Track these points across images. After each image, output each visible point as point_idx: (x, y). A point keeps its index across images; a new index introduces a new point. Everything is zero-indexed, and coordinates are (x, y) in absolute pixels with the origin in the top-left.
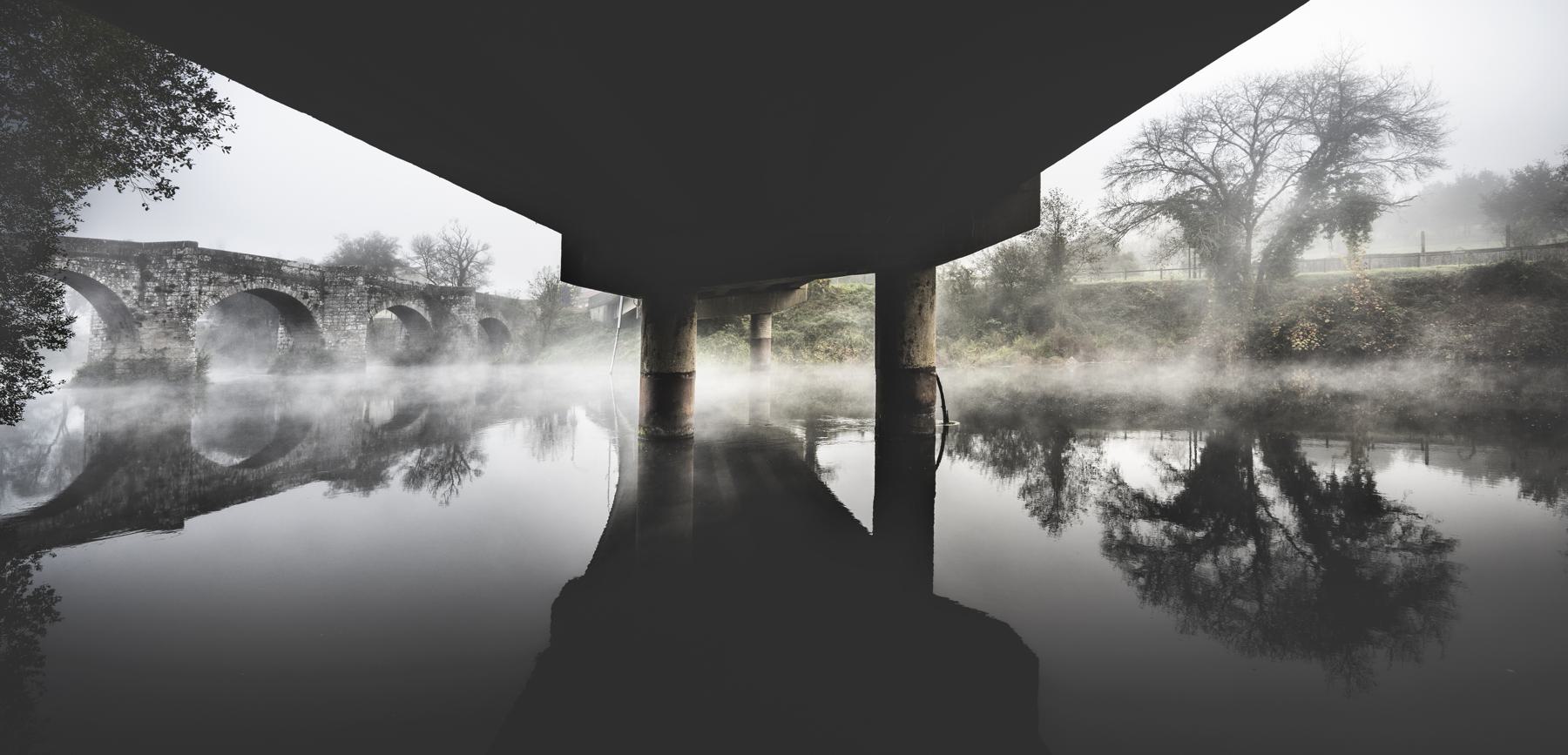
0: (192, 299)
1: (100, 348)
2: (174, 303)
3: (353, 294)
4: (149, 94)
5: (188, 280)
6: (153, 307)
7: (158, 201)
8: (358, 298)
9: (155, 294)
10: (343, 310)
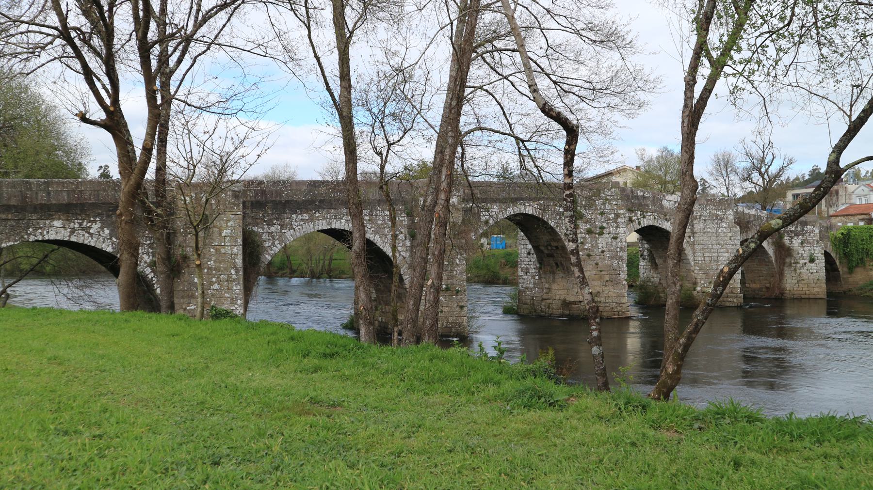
0: (621, 242)
1: (532, 286)
3: (725, 230)
5: (616, 222)
6: (586, 249)
8: (730, 234)
9: (587, 236)
10: (714, 247)
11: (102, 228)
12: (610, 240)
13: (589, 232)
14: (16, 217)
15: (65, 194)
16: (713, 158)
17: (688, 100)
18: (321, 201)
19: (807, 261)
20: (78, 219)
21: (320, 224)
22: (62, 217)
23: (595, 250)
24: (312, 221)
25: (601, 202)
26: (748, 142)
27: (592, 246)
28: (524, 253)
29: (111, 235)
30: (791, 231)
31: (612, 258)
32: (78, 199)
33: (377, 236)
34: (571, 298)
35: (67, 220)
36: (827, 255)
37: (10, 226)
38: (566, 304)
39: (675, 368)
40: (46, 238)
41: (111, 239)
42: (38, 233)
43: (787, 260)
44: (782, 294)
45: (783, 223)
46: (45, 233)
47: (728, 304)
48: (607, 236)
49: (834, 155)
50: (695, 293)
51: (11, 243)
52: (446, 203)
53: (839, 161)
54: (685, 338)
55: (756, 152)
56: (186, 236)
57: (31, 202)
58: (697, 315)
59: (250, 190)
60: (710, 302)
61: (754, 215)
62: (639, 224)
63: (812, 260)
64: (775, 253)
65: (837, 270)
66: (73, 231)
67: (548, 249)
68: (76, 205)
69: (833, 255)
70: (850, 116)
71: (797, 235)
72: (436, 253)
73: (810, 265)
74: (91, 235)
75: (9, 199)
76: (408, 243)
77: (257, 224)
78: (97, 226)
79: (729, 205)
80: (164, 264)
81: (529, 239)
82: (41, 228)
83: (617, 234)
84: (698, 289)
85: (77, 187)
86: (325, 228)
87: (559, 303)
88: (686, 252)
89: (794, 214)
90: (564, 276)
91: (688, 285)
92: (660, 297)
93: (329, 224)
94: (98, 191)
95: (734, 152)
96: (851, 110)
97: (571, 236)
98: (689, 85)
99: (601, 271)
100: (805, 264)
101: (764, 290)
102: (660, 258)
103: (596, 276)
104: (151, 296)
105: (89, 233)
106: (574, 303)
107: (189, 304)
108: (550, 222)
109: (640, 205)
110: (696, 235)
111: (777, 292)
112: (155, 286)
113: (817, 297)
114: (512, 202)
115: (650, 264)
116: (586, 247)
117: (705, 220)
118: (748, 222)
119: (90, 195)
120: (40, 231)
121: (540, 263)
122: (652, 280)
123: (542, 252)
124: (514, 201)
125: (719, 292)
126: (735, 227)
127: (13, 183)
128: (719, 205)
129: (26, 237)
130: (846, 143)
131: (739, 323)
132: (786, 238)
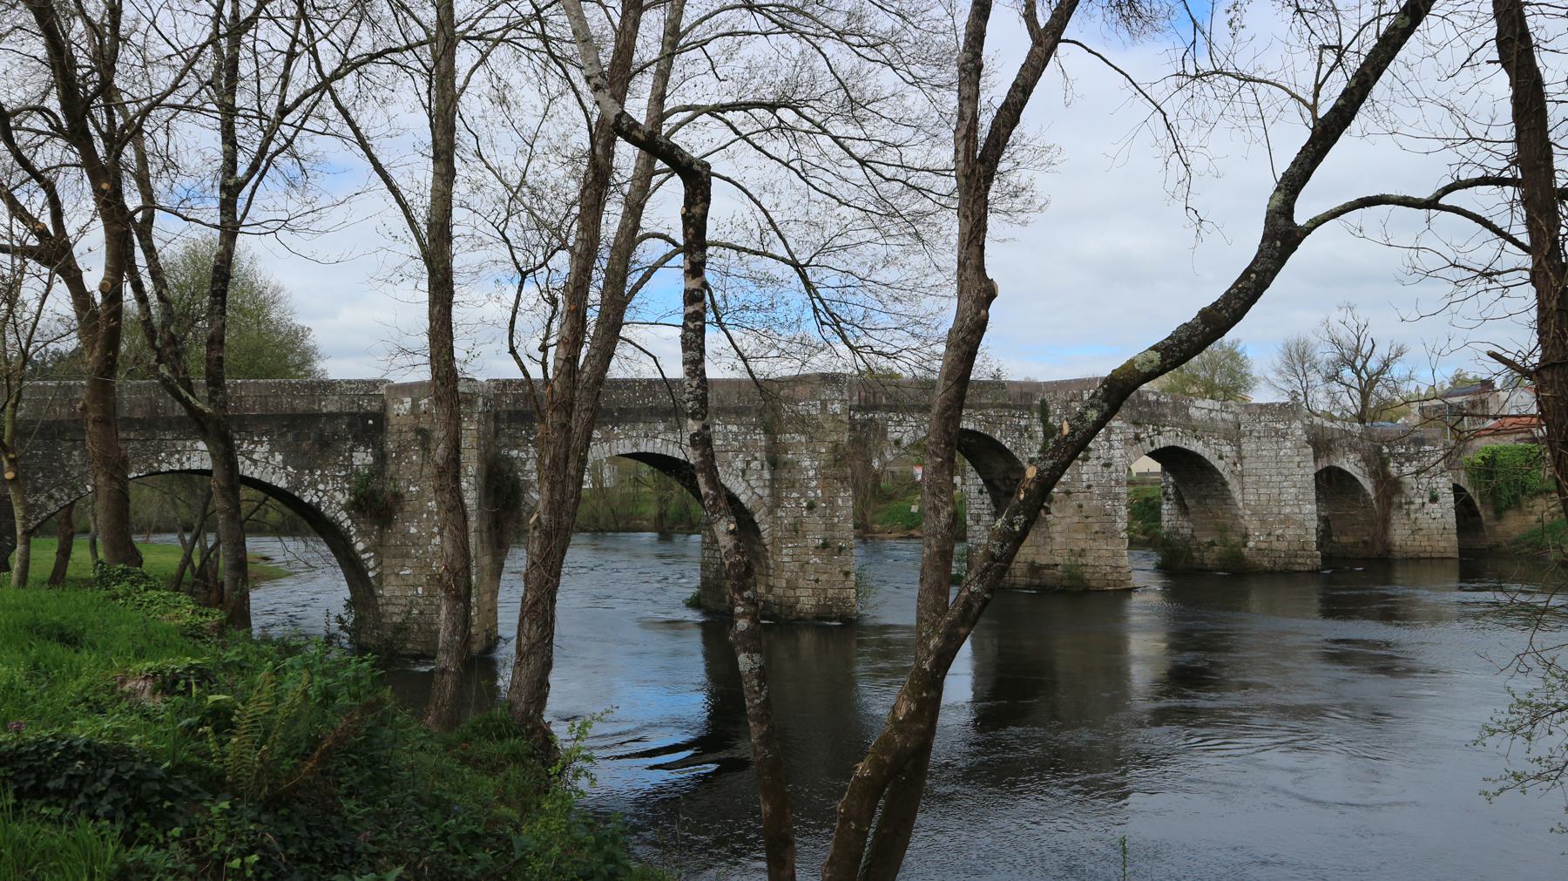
2: (1092, 478)
3: (1289, 452)
4: (312, 473)
5: (1108, 440)
6: (1064, 483)
8: (1298, 459)
10: (1274, 479)
11: (271, 452)
16: (1281, 348)
17: (965, 103)
19: (1426, 500)
23: (1077, 484)
24: (607, 441)
26: (1334, 321)
27: (1072, 479)
28: (974, 489)
29: (285, 463)
31: (1103, 496)
34: (1042, 560)
36: (1457, 489)
39: (913, 707)
40: (186, 466)
41: (285, 468)
43: (1396, 500)
44: (1389, 551)
45: (1163, 359)
46: (184, 459)
47: (1297, 568)
48: (1095, 462)
49: (1280, 196)
50: (1245, 551)
52: (568, 366)
53: (1291, 211)
54: (940, 636)
56: (400, 463)
58: (969, 583)
59: (507, 395)
60: (997, 551)
61: (1340, 431)
62: (1152, 444)
63: (1434, 499)
64: (1376, 489)
65: (1476, 513)
69: (1470, 490)
70: (1313, 108)
71: (1409, 459)
72: (547, 462)
73: (1430, 507)
74: (255, 462)
76: (767, 475)
77: (517, 446)
78: (263, 449)
79: (1294, 413)
80: (224, 496)
81: (978, 470)
82: (178, 452)
84: (1251, 544)
86: (629, 451)
89: (1189, 337)
91: (1235, 539)
92: (1194, 558)
93: (636, 445)
94: (266, 397)
95: (1313, 339)
96: (1316, 95)
97: (690, 404)
98: (964, 70)
100: (1423, 504)
101: (1361, 545)
102: (1192, 497)
105: (251, 459)
106: (1047, 567)
108: (1004, 442)
109: (1152, 414)
111: (1379, 549)
112: (354, 539)
113: (1445, 555)
115: (1175, 506)
117: (1259, 438)
118: (1330, 441)
121: (996, 506)
122: (1181, 531)
125: (1017, 528)
128: (1279, 414)
130: (1306, 166)
131: (1315, 603)
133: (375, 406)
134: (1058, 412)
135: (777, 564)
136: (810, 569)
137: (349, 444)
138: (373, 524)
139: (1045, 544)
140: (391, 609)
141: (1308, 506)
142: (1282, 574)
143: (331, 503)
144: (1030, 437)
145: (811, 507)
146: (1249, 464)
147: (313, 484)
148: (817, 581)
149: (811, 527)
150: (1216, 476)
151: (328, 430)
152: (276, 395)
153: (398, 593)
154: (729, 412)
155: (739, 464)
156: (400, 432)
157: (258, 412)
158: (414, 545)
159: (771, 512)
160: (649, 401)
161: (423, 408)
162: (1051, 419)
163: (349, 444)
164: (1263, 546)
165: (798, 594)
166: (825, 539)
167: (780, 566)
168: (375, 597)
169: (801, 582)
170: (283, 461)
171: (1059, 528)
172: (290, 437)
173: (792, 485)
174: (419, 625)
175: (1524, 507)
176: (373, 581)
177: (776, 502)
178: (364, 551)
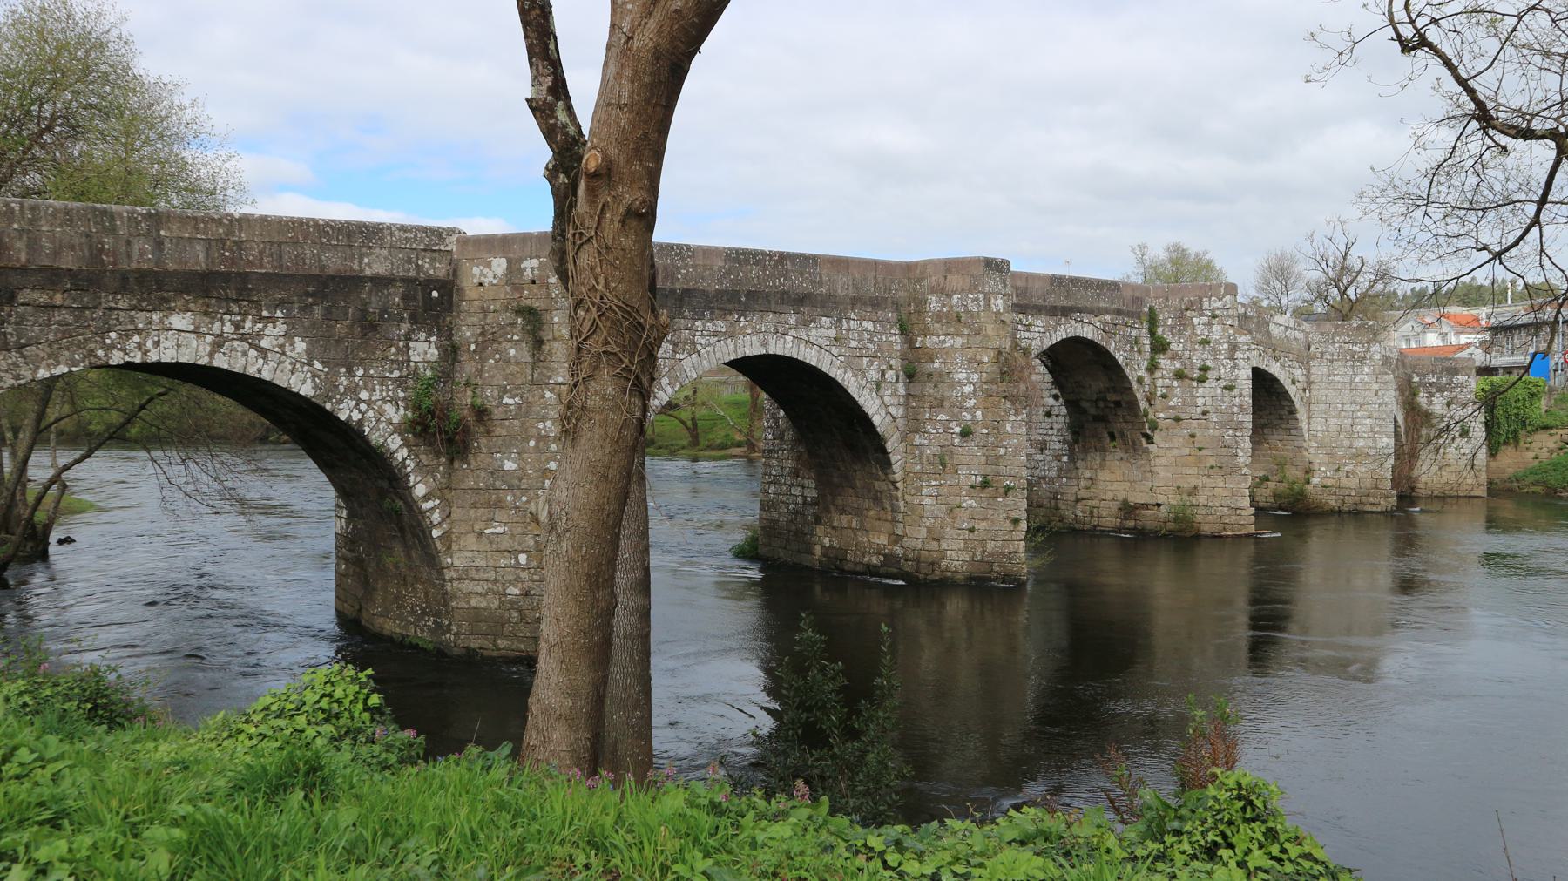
1: (1053, 474)
2: (1209, 401)
4: (350, 372)
5: (1232, 358)
6: (1173, 408)
7: (1342, 219)
8: (1376, 386)
9: (1175, 384)
10: (1347, 407)
11: (290, 336)
12: (1219, 392)
13: (1179, 375)
14: (74, 300)
15: (198, 247)
18: (749, 294)
20: (231, 313)
21: (748, 344)
22: (192, 306)
23: (1190, 409)
25: (1205, 319)
30: (1430, 384)
31: (1222, 425)
32: (233, 261)
33: (849, 373)
34: (1137, 498)
35: (206, 314)
37: (58, 323)
38: (1128, 509)
41: (309, 364)
42: (131, 346)
44: (1413, 489)
46: (149, 344)
47: (1368, 508)
48: (1214, 384)
50: (1309, 487)
51: (62, 369)
55: (1333, 253)
56: (483, 361)
57: (114, 263)
64: (1406, 419)
66: (219, 342)
67: (1097, 407)
68: (226, 277)
71: (1441, 390)
74: (263, 352)
75: (56, 253)
76: (902, 391)
78: (276, 332)
82: (138, 331)
83: (1235, 381)
84: (1315, 480)
85: (230, 233)
87: (1114, 507)
88: (1298, 416)
90: (1125, 456)
91: (1294, 473)
93: (764, 344)
94: (280, 244)
99: (1200, 449)
103: (1190, 458)
104: (400, 503)
105: (258, 348)
106: (1146, 506)
107: (490, 521)
110: (1313, 386)
112: (412, 478)
114: (1063, 315)
116: (1171, 404)
117: (1332, 361)
119: (261, 253)
120: (136, 339)
123: (1084, 412)
124: (1066, 312)
126: (1386, 373)
127: (67, 212)
129: (100, 353)
132: (1421, 395)
133: (439, 270)
134: (1170, 322)
135: (912, 508)
136: (963, 515)
137: (405, 327)
138: (438, 454)
139: (1144, 479)
140: (467, 586)
141: (1385, 440)
142: (1353, 516)
143: (378, 421)
144: (1139, 351)
145: (966, 433)
146: (1315, 391)
147: (353, 391)
148: (972, 530)
149: (966, 460)
150: (1285, 403)
151: (375, 303)
152: (295, 243)
153: (480, 562)
154: (864, 304)
155: (874, 375)
156: (485, 311)
157: (268, 268)
158: (511, 488)
159: (904, 439)
160: (781, 284)
161: (528, 274)
162: (1159, 331)
163: (405, 327)
164: (1329, 482)
165: (944, 545)
166: (985, 476)
167: (917, 511)
168: (440, 571)
169: (949, 532)
170: (308, 352)
171: (1163, 461)
172: (318, 312)
173: (939, 404)
174: (520, 611)
175: (1522, 443)
176: (438, 543)
177: (914, 425)
178: (426, 498)
